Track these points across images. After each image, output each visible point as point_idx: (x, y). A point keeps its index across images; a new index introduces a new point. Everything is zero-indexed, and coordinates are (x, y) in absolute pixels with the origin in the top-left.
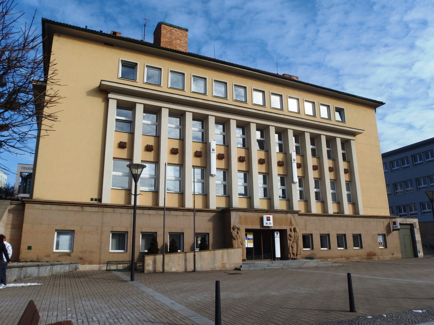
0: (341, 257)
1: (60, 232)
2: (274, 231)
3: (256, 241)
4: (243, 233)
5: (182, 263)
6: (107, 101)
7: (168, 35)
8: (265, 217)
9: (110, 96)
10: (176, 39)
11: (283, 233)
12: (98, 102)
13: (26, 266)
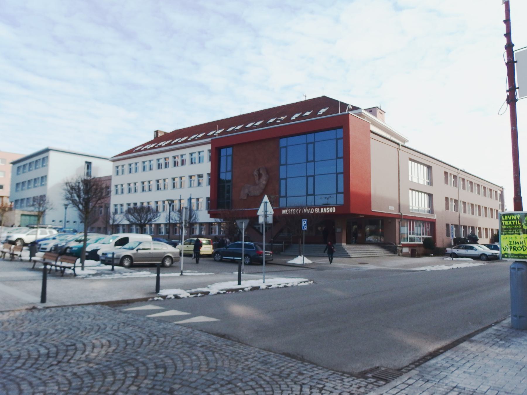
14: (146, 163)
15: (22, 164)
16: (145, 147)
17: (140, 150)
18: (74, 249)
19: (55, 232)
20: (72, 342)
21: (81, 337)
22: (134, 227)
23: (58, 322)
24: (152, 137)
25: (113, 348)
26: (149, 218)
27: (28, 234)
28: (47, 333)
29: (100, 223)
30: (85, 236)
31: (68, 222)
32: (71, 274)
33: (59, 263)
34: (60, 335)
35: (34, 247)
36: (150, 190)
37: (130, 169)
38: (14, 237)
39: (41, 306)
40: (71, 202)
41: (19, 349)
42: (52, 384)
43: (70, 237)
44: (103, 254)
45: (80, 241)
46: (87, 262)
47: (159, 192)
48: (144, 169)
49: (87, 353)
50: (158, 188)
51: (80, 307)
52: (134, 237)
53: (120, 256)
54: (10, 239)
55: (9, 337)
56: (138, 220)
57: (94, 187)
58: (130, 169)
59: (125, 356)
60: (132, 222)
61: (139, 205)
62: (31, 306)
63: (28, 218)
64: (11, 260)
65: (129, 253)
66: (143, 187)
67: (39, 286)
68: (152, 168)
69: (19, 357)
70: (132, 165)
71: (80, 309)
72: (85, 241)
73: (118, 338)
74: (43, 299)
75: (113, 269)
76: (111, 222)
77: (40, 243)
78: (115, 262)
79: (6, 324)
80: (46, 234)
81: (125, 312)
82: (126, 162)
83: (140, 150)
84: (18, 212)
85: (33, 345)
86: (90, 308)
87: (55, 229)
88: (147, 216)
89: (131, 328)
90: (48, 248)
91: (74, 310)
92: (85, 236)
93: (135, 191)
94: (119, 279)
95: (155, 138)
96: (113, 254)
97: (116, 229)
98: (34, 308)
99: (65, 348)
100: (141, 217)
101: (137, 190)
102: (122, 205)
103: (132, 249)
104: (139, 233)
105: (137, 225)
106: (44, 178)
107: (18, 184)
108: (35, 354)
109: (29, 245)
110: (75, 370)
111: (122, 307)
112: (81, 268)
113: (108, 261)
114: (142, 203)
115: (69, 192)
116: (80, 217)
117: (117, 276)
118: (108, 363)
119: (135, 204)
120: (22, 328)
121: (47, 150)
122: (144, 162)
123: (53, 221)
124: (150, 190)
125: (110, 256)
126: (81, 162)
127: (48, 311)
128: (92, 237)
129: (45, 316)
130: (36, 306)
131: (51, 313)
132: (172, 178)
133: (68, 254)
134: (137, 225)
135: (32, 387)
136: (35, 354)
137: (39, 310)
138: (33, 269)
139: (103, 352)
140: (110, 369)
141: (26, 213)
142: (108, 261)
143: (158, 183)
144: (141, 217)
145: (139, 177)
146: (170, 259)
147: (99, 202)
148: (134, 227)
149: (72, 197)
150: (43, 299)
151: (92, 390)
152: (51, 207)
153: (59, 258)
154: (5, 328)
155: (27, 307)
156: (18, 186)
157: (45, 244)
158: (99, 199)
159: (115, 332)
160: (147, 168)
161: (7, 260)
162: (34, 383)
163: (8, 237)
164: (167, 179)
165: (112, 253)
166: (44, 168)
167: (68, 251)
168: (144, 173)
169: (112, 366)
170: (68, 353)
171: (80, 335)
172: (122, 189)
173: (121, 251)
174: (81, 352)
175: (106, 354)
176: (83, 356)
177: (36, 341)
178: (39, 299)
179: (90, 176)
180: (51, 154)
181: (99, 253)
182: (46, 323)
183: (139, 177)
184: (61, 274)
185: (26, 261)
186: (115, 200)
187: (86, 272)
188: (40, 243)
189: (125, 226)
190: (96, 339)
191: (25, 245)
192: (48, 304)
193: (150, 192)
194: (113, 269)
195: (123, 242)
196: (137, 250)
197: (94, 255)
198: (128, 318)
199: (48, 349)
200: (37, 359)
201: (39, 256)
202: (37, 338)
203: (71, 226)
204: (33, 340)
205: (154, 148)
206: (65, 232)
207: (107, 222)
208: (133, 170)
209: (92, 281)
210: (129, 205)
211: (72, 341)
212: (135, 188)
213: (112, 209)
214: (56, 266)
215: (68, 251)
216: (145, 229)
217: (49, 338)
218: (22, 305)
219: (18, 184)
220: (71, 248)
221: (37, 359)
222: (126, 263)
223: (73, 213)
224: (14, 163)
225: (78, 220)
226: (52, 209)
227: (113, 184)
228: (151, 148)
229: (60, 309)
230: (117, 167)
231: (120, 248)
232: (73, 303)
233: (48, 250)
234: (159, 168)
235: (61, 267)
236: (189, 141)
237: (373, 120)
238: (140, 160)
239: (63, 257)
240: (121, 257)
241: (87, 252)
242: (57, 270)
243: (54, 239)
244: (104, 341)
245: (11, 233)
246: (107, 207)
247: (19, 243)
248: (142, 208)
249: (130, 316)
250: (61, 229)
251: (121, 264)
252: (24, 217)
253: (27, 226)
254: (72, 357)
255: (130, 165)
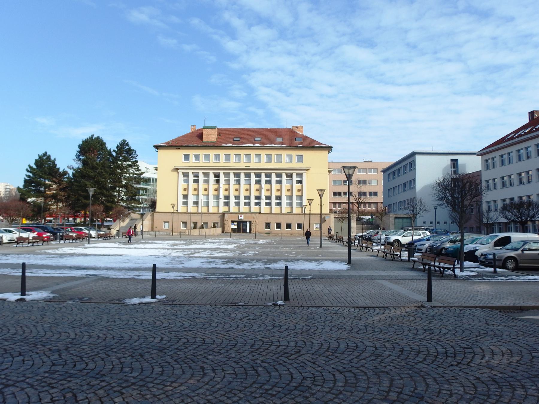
0: (287, 233)
1: (165, 222)
2: (246, 222)
3: (238, 226)
4: (230, 222)
5: (198, 232)
6: (178, 173)
7: (206, 134)
8: (240, 216)
9: (179, 171)
10: (210, 134)
11: (250, 222)
12: (175, 173)
13: (400, 278)
14: (522, 151)
15: (391, 171)
16: (519, 134)
17: (512, 138)
18: (449, 249)
19: (428, 233)
20: (467, 345)
21: (477, 341)
22: (512, 225)
23: (448, 323)
24: (526, 120)
25: (516, 358)
26: (531, 214)
27: (404, 236)
28: (440, 332)
29: (473, 222)
30: (462, 236)
31: (438, 223)
32: (450, 275)
33: (437, 264)
34: (454, 336)
35: (411, 247)
36: (529, 182)
37: (502, 161)
38: (393, 238)
39: (428, 305)
40: (445, 202)
41: (418, 344)
42: (456, 384)
43: (444, 238)
44: (482, 255)
45: (455, 242)
46: (467, 264)
47: (522, 186)
48: (520, 159)
49: (487, 359)
50: (521, 182)
51: (467, 309)
52: (516, 236)
53: (502, 257)
54: (388, 241)
55: (406, 332)
56: (518, 217)
57: (468, 184)
58: (502, 161)
59: (533, 369)
60: (510, 219)
61: (516, 200)
62: (420, 304)
63: (401, 220)
64: (392, 260)
65: (512, 254)
66: (520, 179)
67: (424, 286)
68: (529, 155)
69: (419, 352)
70: (504, 156)
71: (468, 312)
72: (462, 240)
73: (520, 349)
74: (430, 299)
75: (495, 272)
76: (485, 220)
77: (415, 244)
78: (497, 263)
79: (400, 319)
80: (420, 235)
81: (521, 320)
82: (497, 154)
83: (512, 138)
84: (392, 216)
85: (429, 342)
86: (478, 312)
87: (426, 230)
88: (529, 212)
89: (534, 339)
90: (424, 248)
91: (462, 312)
92: (462, 236)
93: (511, 184)
94: (503, 283)
95: (530, 120)
96: (494, 255)
97: (490, 228)
98: (422, 306)
99: (462, 350)
100: (521, 213)
101: (512, 184)
102: (495, 202)
103: (516, 250)
104: (520, 232)
105: (515, 222)
106: (412, 182)
107: (389, 190)
108: (433, 352)
109: (406, 246)
110: (478, 375)
111: (515, 314)
112: (459, 269)
113: (485, 261)
114: (521, 198)
115: (441, 191)
116: (451, 216)
117: (501, 279)
118: (514, 374)
119: (512, 199)
120: (415, 324)
121: (413, 154)
122: (519, 151)
123: (424, 223)
124: (529, 182)
125: (490, 257)
126: (446, 161)
127: (436, 310)
128: (468, 237)
129: (433, 316)
130: (424, 305)
131: (440, 313)
132: (518, 174)
133: (443, 255)
134: (515, 222)
135: (438, 384)
136: (433, 352)
137: (427, 308)
138: (413, 269)
139: (505, 361)
140: (518, 380)
141: (398, 216)
142: (485, 261)
143: (521, 177)
144: (521, 213)
145: (504, 171)
146: (514, 261)
147: (474, 200)
148: (512, 225)
149: (445, 197)
150: (430, 299)
151: (501, 399)
152: (424, 209)
153: (437, 259)
154: (400, 322)
155: (416, 305)
156: (389, 191)
157: (421, 245)
158: (474, 197)
159: (513, 340)
160: (524, 157)
161: (389, 260)
162: (438, 379)
163: (386, 239)
164: (513, 175)
165: (493, 254)
166: (411, 172)
167: (444, 252)
168: (520, 163)
169: (519, 378)
170: (466, 355)
171: (474, 339)
172: (495, 184)
173: (504, 252)
174: (480, 357)
175: (509, 364)
176: (483, 361)
177: (431, 339)
178: (425, 298)
179: (457, 173)
180: (418, 157)
181: (478, 253)
182: (436, 322)
183: (504, 171)
184: (442, 275)
185: (405, 261)
186: (488, 197)
187: (465, 273)
188: (415, 244)
189: (502, 224)
190: (494, 345)
191: (402, 246)
192: (434, 303)
193: (530, 184)
194: (495, 272)
195: (505, 241)
196: (523, 251)
197: (471, 256)
198: (527, 326)
199: (446, 348)
200: (436, 357)
201: (417, 256)
202: (432, 336)
203: (442, 227)
204: (429, 337)
205: (530, 132)
206: (436, 233)
207: (481, 221)
208: (491, 166)
209: (475, 283)
210: (504, 200)
211: (468, 343)
212: (511, 181)
213: (485, 207)
214: (435, 267)
215: (444, 252)
216: (527, 227)
217: (444, 337)
218: (411, 302)
219: (389, 190)
220: (447, 249)
221: (436, 357)
222: (510, 265)
223: (444, 213)
224: (384, 171)
225: (449, 221)
226: (425, 210)
227: (484, 178)
228: (526, 134)
229: (447, 309)
230: (487, 161)
231: (501, 249)
232: (460, 305)
233: (424, 250)
234: (503, 165)
235: (439, 268)
236: (534, 131)
237: (112, 274)
238: (513, 149)
239: (441, 257)
240: (503, 259)
241: (465, 253)
242: (435, 271)
243: (428, 240)
244: (504, 349)
245: (388, 235)
246: (480, 206)
247: (396, 244)
248: (521, 204)
249: (528, 324)
250: (433, 230)
251: (504, 266)
252: (397, 220)
253: (402, 229)
254: (472, 360)
255: (502, 156)
